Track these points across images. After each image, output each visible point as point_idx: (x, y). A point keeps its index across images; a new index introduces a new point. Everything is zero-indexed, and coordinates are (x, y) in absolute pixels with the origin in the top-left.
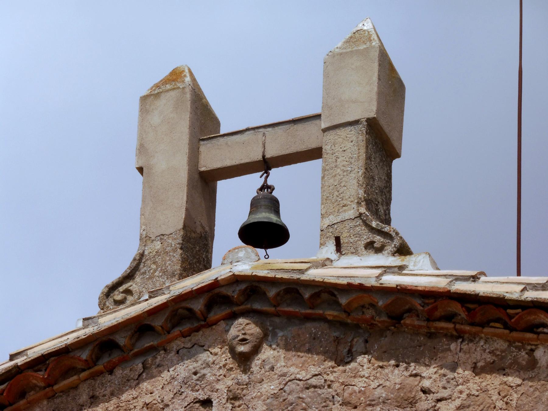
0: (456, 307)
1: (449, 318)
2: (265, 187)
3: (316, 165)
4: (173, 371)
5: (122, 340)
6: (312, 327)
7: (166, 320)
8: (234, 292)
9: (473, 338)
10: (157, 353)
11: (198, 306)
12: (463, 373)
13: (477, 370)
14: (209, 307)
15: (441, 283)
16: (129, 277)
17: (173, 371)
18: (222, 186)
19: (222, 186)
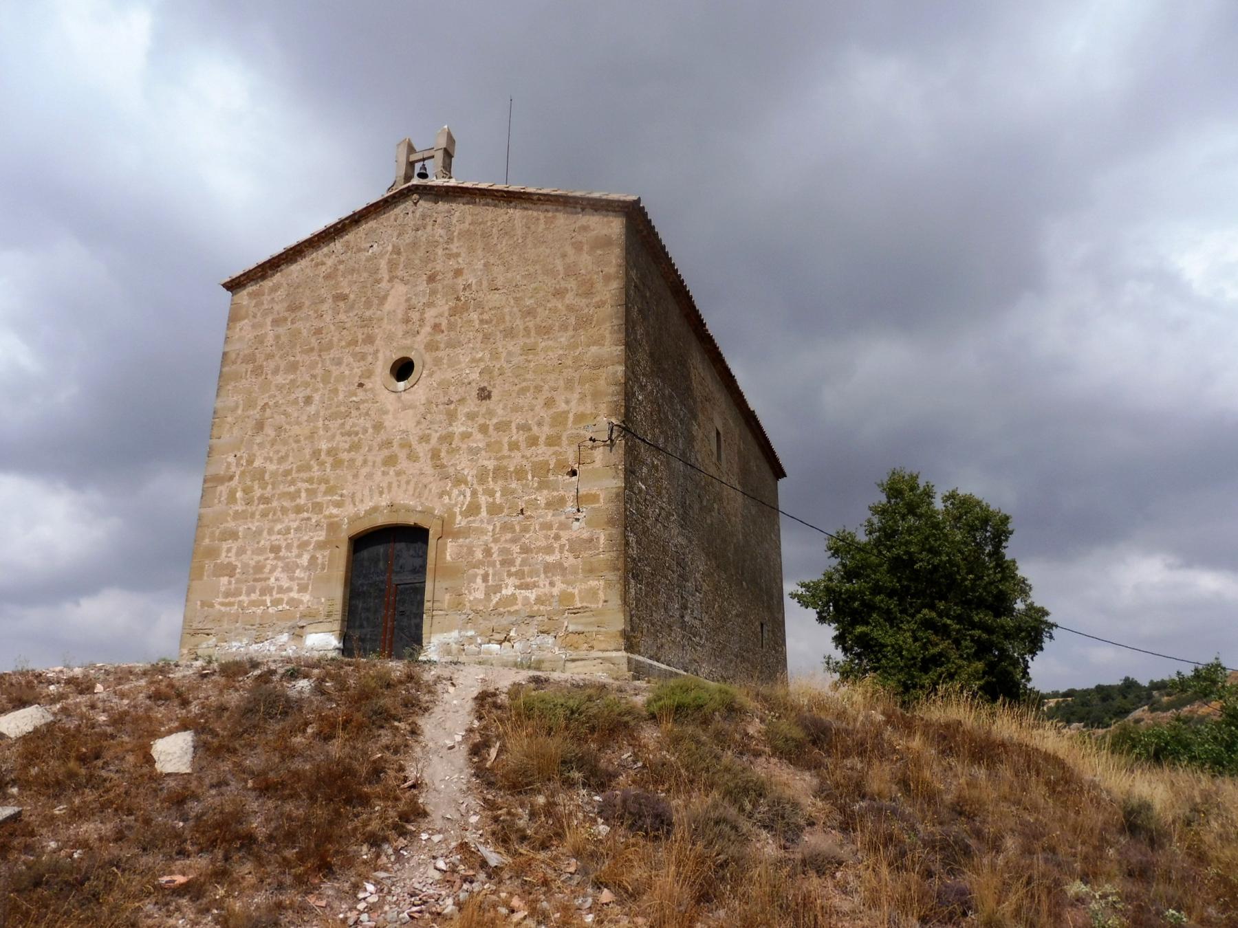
0: (458, 190)
1: (458, 192)
2: (424, 165)
3: (432, 160)
4: (354, 494)
5: (389, 200)
6: (430, 196)
7: (368, 882)
8: (413, 188)
9: (463, 197)
10: (738, 487)
11: (405, 192)
12: (461, 205)
13: (464, 204)
14: (408, 192)
15: (456, 184)
16: (393, 186)
17: (354, 494)
18: (416, 164)
19: (416, 164)
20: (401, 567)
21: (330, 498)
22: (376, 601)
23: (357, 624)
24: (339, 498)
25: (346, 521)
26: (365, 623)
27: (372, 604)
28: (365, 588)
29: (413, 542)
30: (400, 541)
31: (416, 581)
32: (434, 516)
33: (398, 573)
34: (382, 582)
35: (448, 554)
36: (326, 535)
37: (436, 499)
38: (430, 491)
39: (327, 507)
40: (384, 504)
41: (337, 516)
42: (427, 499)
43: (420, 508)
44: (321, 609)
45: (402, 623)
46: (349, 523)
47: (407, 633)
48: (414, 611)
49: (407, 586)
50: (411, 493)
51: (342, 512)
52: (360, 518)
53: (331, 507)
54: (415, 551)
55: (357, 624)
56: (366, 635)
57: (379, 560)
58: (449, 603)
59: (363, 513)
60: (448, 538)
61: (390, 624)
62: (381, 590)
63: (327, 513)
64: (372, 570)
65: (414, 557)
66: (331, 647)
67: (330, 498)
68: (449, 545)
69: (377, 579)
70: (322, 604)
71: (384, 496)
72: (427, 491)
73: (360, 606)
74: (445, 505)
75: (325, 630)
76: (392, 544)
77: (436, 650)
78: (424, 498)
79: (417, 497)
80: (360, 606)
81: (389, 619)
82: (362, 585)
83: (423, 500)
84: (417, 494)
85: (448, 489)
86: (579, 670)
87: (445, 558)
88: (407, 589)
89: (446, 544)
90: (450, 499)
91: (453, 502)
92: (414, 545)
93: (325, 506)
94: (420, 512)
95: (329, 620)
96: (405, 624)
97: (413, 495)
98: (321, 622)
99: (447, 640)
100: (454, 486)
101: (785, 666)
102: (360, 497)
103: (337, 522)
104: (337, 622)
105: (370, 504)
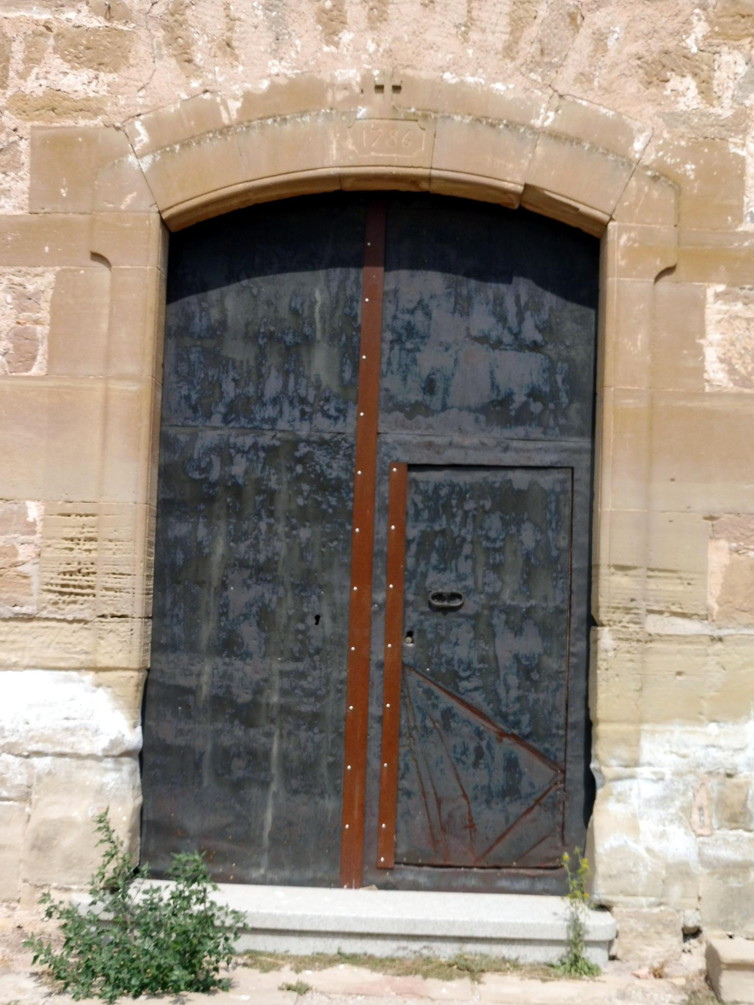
20: (429, 387)
21: (45, 16)
22: (304, 533)
23: (207, 631)
24: (97, 22)
25: (143, 137)
26: (249, 632)
27: (281, 546)
28: (239, 468)
29: (483, 274)
30: (416, 264)
31: (508, 459)
32: (633, 167)
33: (413, 410)
34: (330, 446)
35: (711, 355)
36: (33, 193)
37: (632, 87)
38: (600, 39)
39: (31, 60)
40: (350, 74)
41: (88, 108)
42: (584, 78)
43: (546, 119)
44: (25, 553)
45: (445, 650)
46: (157, 147)
47: (478, 698)
48: (506, 598)
49: (463, 478)
50: (499, 39)
51: (114, 90)
52: (224, 130)
53: (56, 62)
54: (502, 319)
55: (207, 631)
56: (258, 691)
57: (308, 341)
58: (729, 588)
59: (235, 105)
60: (707, 277)
61: (379, 650)
62: (324, 485)
63: (33, 86)
64: (273, 385)
65: (498, 344)
66: (99, 745)
67: (45, 16)
68: (714, 310)
69: (304, 430)
70: (31, 528)
71: (346, 37)
72: (583, 41)
73: (220, 548)
74: (682, 118)
75: (51, 654)
76: (374, 273)
77: (663, 801)
78: (570, 72)
79: (533, 65)
80: (220, 548)
81: (379, 625)
82: (225, 452)
83: (565, 80)
84: (527, 49)
85: (692, 44)
86: (109, 580)
87: (699, 370)
88: (461, 494)
89: (699, 305)
90: (706, 90)
91: (725, 110)
92: (492, 289)
93: (18, 50)
94: (554, 136)
95: (72, 611)
96: (462, 652)
97: (509, 51)
98: (29, 618)
99: (721, 758)
100: (725, 35)
101: (159, 470)
102: (218, 27)
103: (89, 137)
104: (123, 627)
105: (275, 67)
